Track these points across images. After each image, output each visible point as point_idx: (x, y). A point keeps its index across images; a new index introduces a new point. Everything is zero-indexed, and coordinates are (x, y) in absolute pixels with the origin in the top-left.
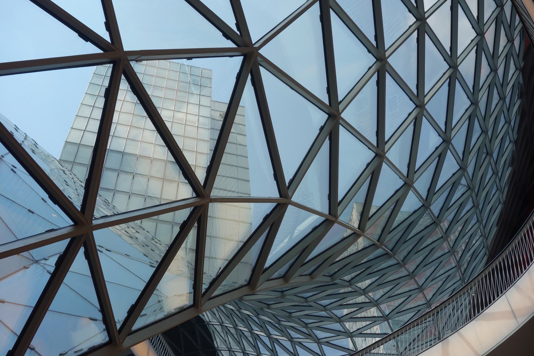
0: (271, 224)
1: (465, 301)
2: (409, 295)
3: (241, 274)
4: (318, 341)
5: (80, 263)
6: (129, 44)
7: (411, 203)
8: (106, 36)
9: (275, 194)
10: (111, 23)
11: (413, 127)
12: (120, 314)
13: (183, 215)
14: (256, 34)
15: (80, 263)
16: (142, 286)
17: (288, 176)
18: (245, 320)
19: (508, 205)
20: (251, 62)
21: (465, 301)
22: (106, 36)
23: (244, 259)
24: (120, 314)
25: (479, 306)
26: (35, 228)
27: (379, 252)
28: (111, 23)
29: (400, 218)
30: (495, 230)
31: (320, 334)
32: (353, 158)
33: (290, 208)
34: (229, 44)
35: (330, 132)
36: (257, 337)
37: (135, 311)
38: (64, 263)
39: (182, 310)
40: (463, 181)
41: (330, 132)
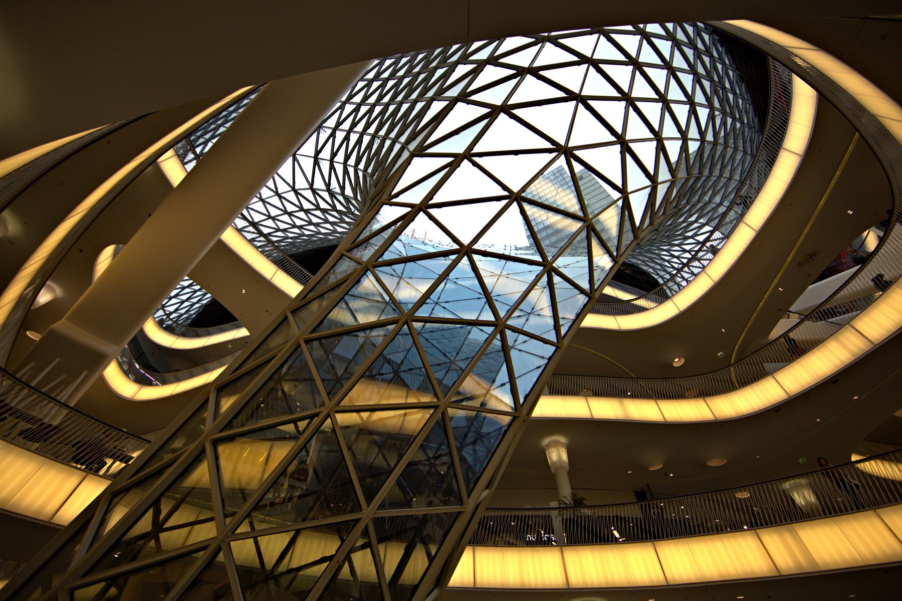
0: (627, 206)
1: (761, 165)
2: (726, 186)
3: (628, 237)
4: (692, 237)
5: (556, 279)
6: (515, 189)
7: (693, 147)
8: (506, 193)
9: (649, 183)
10: (504, 187)
11: (401, 196)
12: (586, 286)
13: (584, 234)
14: (562, 141)
15: (556, 279)
16: (587, 270)
17: (652, 172)
18: (649, 251)
19: (754, 103)
20: (567, 152)
21: (761, 165)
22: (506, 193)
23: (625, 230)
24: (586, 286)
25: (771, 162)
26: (532, 277)
27: (692, 181)
28: (504, 187)
29: (692, 158)
30: (756, 120)
31: (690, 234)
32: (646, 152)
33: (630, 196)
34: (555, 154)
35: (626, 149)
36: (651, 258)
37: (591, 281)
38: (550, 284)
39: (611, 268)
40: (717, 113)
41: (626, 149)
